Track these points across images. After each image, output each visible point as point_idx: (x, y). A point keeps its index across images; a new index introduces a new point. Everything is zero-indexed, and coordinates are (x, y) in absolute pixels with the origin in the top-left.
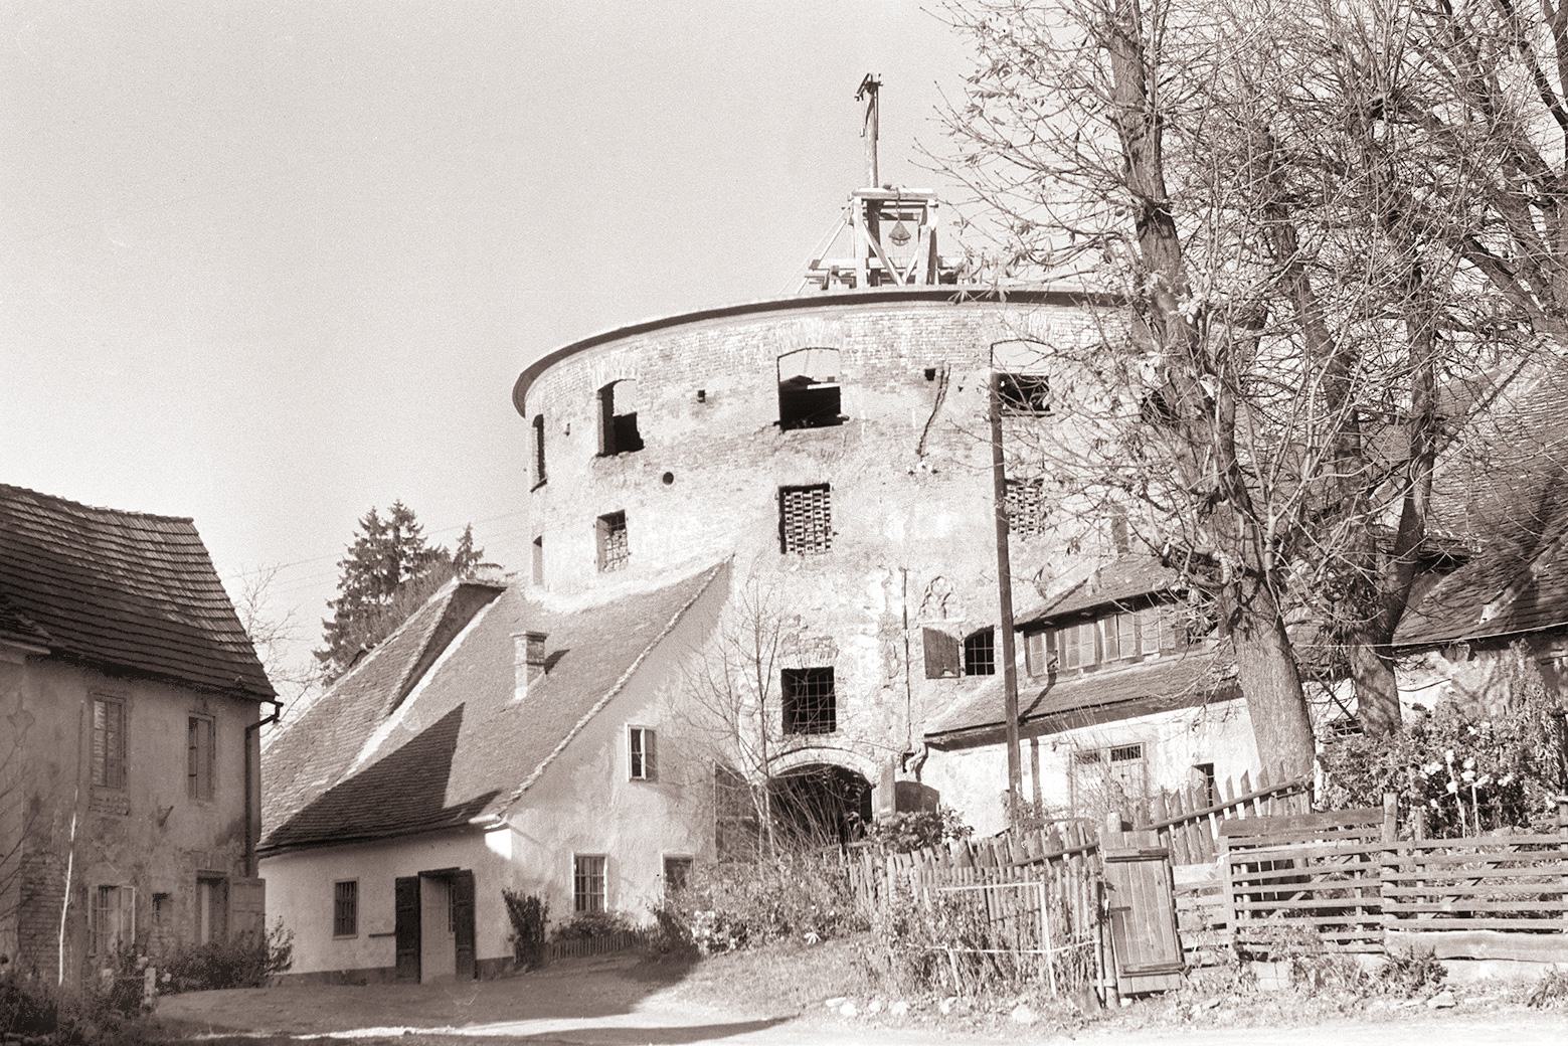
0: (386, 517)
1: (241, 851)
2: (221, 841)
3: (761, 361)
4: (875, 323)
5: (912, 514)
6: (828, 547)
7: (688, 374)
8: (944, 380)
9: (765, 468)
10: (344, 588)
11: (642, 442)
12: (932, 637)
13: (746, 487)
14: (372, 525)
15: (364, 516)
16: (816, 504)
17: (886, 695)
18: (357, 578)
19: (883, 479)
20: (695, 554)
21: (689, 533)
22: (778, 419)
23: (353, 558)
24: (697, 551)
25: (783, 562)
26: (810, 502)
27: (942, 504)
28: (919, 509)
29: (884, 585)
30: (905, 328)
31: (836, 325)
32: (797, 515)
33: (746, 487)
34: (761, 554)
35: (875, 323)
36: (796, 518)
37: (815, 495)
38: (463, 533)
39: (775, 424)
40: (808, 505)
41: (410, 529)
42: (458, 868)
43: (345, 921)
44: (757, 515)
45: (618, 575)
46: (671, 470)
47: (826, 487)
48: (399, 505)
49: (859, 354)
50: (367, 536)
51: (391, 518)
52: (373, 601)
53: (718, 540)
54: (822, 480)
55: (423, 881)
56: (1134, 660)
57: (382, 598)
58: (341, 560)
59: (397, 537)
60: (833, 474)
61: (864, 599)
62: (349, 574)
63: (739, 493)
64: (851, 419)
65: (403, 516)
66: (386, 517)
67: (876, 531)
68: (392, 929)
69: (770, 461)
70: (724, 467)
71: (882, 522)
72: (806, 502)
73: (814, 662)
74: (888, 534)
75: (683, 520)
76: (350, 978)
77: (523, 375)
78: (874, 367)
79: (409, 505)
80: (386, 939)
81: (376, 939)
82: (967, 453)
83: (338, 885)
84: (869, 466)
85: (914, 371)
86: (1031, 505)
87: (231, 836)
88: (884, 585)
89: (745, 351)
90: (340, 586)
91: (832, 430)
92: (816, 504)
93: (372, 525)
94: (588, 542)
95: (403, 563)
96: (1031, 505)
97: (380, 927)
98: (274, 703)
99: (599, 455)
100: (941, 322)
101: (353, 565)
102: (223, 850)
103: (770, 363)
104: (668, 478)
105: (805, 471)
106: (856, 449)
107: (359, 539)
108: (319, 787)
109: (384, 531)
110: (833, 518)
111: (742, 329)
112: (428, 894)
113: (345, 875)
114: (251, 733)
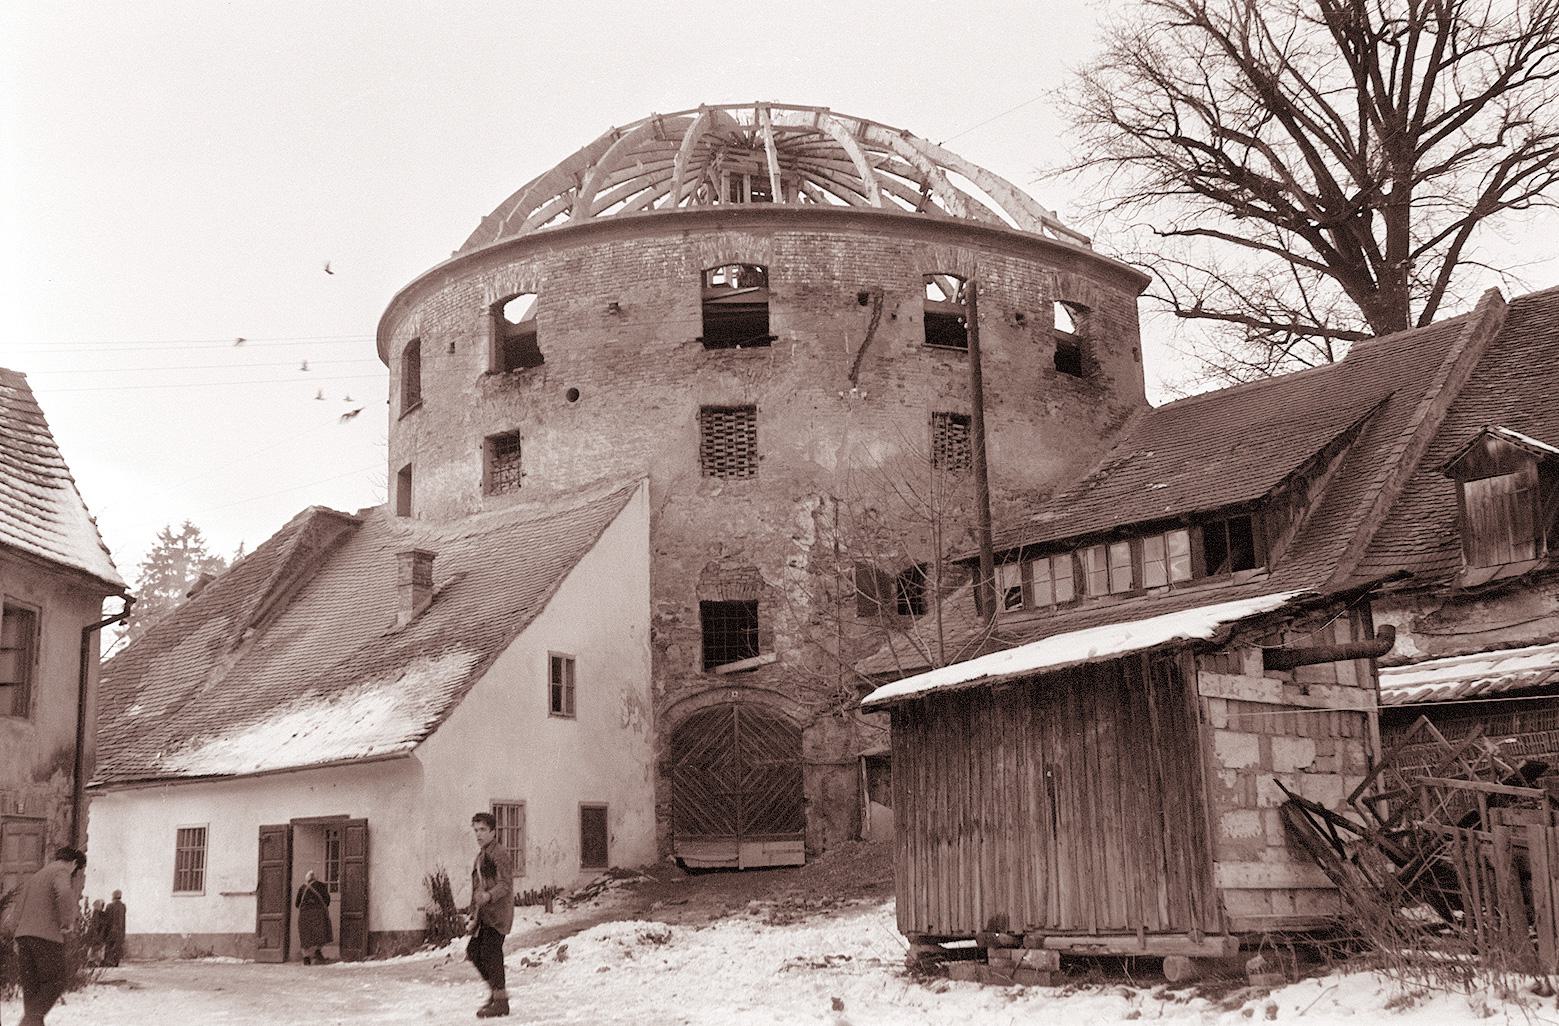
0: (177, 531)
1: (67, 790)
2: (43, 776)
3: (683, 274)
4: (806, 242)
5: (844, 441)
6: (751, 473)
7: (599, 287)
8: (878, 308)
9: (686, 386)
10: (141, 583)
11: (542, 357)
12: (863, 572)
13: (661, 405)
14: (167, 537)
15: (162, 532)
16: (740, 427)
17: (816, 633)
18: (152, 577)
19: (814, 404)
20: (602, 475)
21: (596, 452)
22: (700, 334)
23: (151, 561)
24: (605, 472)
25: (703, 487)
26: (732, 424)
27: (875, 433)
28: (852, 437)
29: (814, 514)
30: (838, 251)
31: (765, 242)
32: (717, 438)
33: (661, 405)
34: (681, 477)
35: (806, 242)
36: (716, 441)
37: (738, 417)
38: (238, 548)
39: (698, 340)
40: (731, 428)
41: (196, 541)
42: (347, 817)
43: (189, 874)
44: (674, 434)
45: (506, 499)
46: (576, 385)
47: (751, 409)
48: (188, 523)
49: (789, 273)
50: (161, 544)
51: (182, 532)
52: (164, 595)
53: (630, 461)
54: (750, 400)
55: (297, 831)
56: (1128, 595)
57: (171, 593)
58: (140, 562)
59: (185, 547)
60: (761, 395)
61: (794, 529)
62: (146, 574)
63: (655, 411)
64: (781, 339)
65: (191, 531)
66: (177, 531)
67: (806, 457)
68: (253, 887)
69: (691, 379)
70: (639, 384)
71: (812, 448)
72: (728, 424)
73: (736, 595)
74: (819, 461)
75: (590, 439)
76: (196, 949)
77: (397, 299)
78: (805, 287)
79: (195, 524)
80: (243, 899)
81: (228, 898)
82: (900, 382)
83: (182, 832)
84: (800, 388)
85: (848, 294)
86: (959, 442)
87: (55, 770)
88: (814, 514)
89: (665, 264)
90: (138, 582)
91: (762, 350)
92: (740, 427)
93: (167, 537)
94: (473, 466)
95: (190, 566)
96: (959, 442)
97: (237, 886)
98: (124, 596)
99: (489, 374)
100: (874, 246)
101: (150, 567)
102: (43, 789)
103: (693, 276)
104: (574, 395)
105: (728, 389)
106: (785, 371)
107: (155, 547)
108: (1038, 525)
109: (174, 541)
110: (760, 440)
111: (662, 241)
112: (301, 844)
113: (192, 821)
114: (89, 634)
